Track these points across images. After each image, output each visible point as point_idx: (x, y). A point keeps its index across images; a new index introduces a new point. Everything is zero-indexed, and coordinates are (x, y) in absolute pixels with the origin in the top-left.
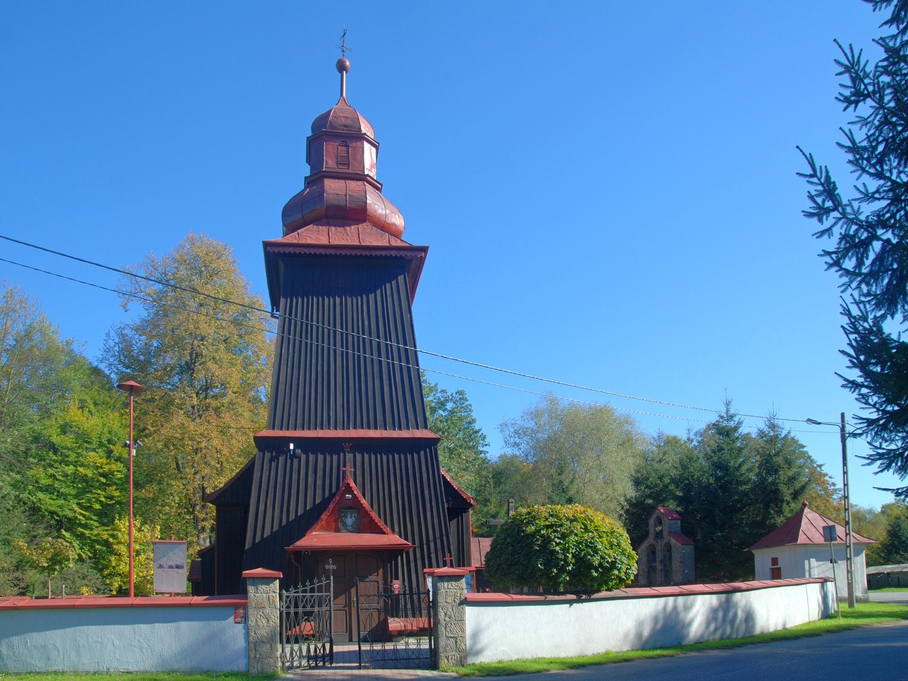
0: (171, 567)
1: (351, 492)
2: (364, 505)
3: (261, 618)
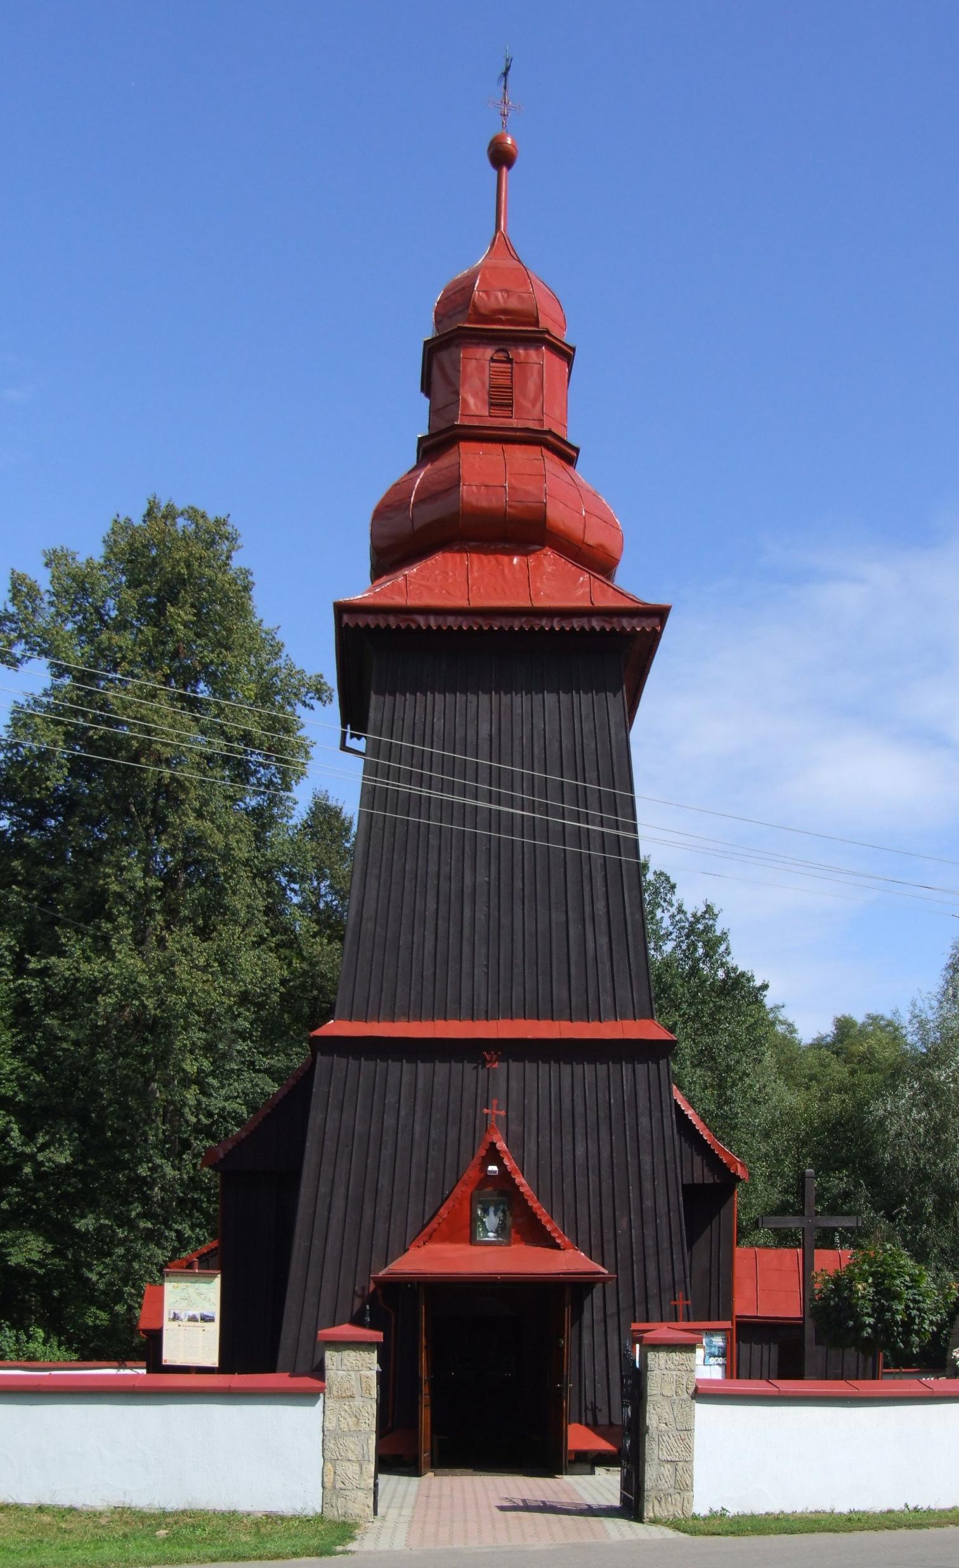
0: (193, 1319)
1: (499, 1162)
2: (522, 1189)
3: (347, 1416)
